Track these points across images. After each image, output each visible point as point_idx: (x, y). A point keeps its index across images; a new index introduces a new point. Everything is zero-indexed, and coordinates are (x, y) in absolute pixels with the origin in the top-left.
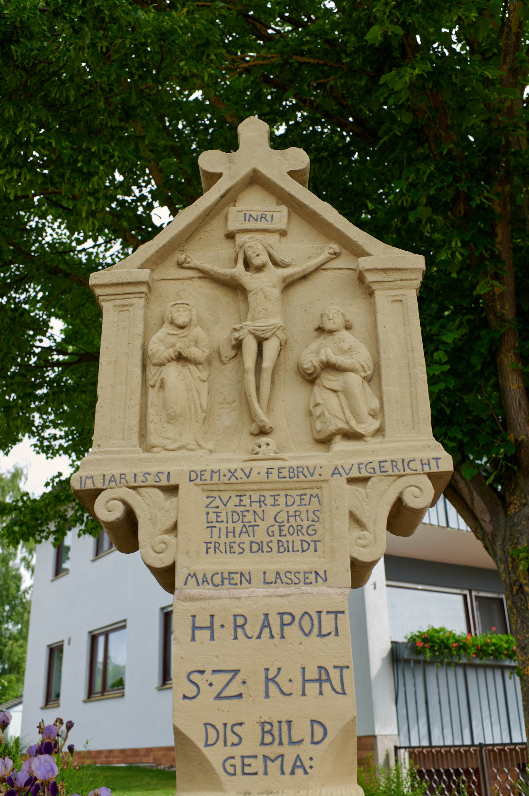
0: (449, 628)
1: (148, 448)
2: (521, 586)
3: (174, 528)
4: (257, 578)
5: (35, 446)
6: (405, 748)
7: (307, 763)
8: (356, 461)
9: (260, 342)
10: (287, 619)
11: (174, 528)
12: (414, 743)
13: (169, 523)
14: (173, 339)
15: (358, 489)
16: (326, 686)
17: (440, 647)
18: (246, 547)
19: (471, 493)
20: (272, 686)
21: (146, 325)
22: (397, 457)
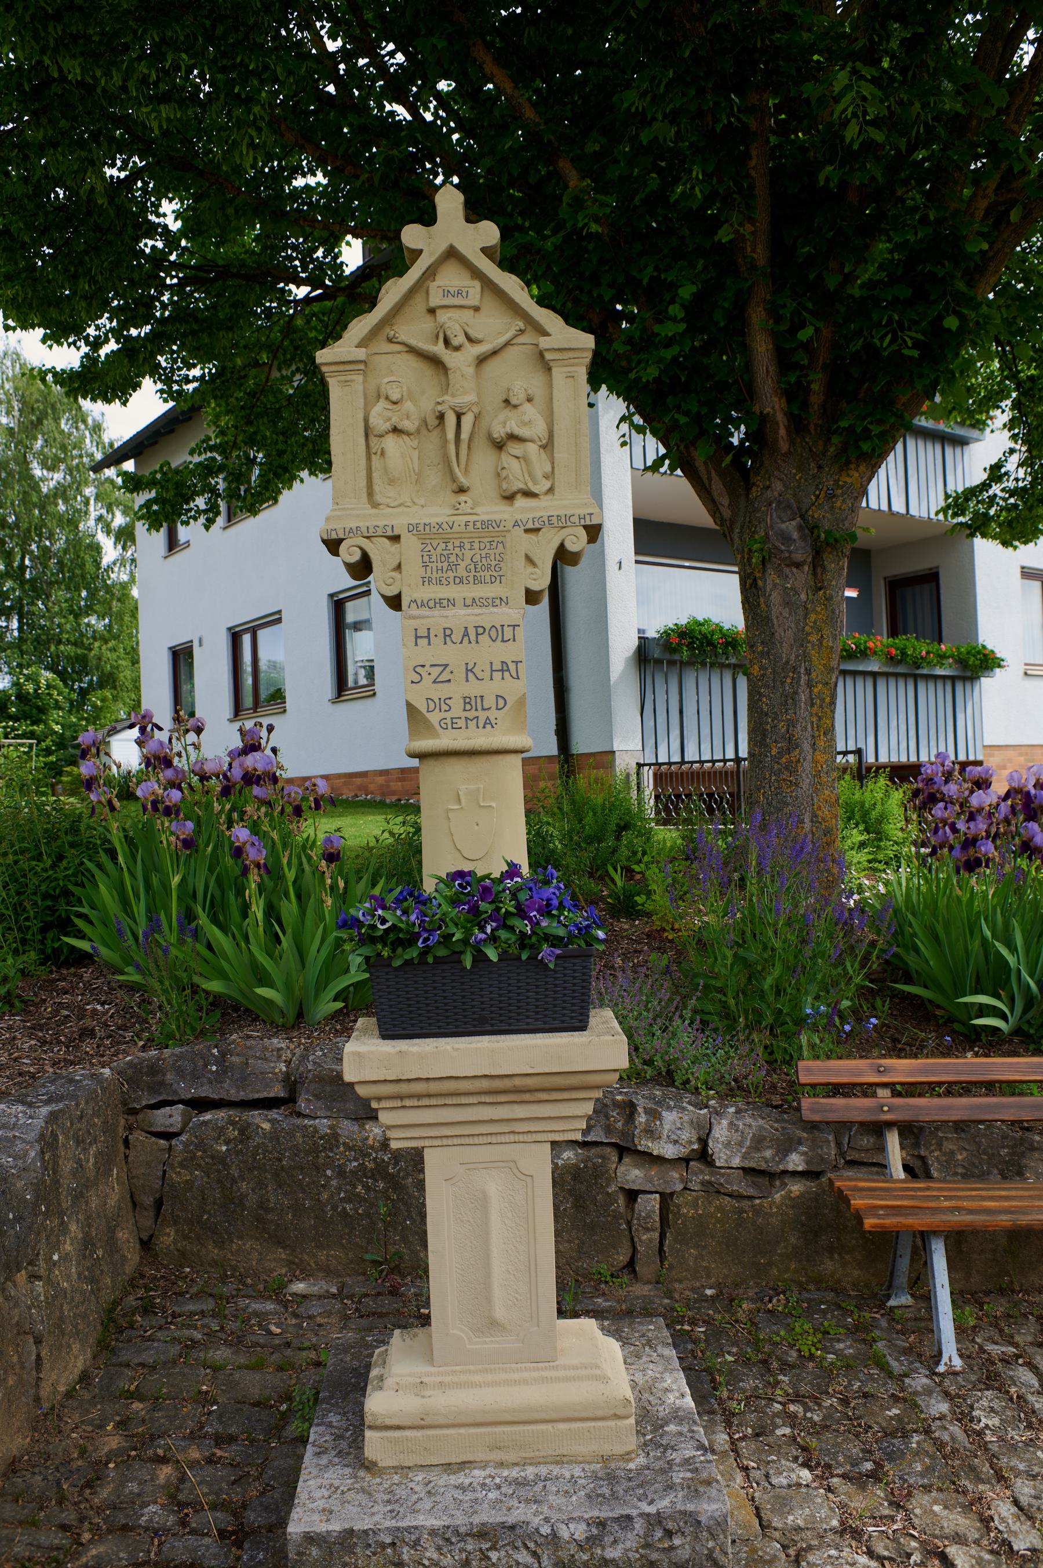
0: (715, 620)
1: (375, 505)
2: (755, 580)
3: (399, 567)
4: (459, 603)
5: (162, 391)
6: (650, 765)
7: (493, 722)
8: (531, 516)
9: (459, 417)
10: (480, 630)
11: (399, 567)
12: (663, 758)
13: (395, 564)
14: (389, 414)
15: (532, 537)
16: (506, 674)
17: (702, 643)
18: (451, 580)
19: (709, 473)
20: (470, 674)
21: (365, 398)
22: (562, 513)
